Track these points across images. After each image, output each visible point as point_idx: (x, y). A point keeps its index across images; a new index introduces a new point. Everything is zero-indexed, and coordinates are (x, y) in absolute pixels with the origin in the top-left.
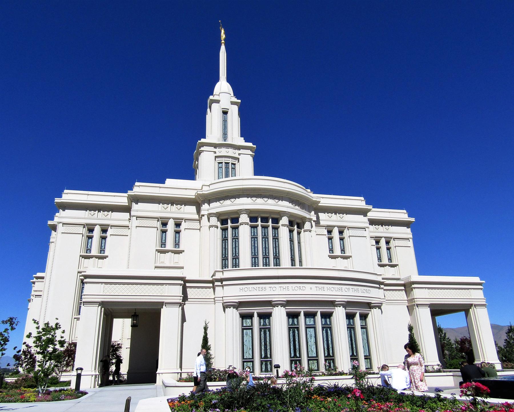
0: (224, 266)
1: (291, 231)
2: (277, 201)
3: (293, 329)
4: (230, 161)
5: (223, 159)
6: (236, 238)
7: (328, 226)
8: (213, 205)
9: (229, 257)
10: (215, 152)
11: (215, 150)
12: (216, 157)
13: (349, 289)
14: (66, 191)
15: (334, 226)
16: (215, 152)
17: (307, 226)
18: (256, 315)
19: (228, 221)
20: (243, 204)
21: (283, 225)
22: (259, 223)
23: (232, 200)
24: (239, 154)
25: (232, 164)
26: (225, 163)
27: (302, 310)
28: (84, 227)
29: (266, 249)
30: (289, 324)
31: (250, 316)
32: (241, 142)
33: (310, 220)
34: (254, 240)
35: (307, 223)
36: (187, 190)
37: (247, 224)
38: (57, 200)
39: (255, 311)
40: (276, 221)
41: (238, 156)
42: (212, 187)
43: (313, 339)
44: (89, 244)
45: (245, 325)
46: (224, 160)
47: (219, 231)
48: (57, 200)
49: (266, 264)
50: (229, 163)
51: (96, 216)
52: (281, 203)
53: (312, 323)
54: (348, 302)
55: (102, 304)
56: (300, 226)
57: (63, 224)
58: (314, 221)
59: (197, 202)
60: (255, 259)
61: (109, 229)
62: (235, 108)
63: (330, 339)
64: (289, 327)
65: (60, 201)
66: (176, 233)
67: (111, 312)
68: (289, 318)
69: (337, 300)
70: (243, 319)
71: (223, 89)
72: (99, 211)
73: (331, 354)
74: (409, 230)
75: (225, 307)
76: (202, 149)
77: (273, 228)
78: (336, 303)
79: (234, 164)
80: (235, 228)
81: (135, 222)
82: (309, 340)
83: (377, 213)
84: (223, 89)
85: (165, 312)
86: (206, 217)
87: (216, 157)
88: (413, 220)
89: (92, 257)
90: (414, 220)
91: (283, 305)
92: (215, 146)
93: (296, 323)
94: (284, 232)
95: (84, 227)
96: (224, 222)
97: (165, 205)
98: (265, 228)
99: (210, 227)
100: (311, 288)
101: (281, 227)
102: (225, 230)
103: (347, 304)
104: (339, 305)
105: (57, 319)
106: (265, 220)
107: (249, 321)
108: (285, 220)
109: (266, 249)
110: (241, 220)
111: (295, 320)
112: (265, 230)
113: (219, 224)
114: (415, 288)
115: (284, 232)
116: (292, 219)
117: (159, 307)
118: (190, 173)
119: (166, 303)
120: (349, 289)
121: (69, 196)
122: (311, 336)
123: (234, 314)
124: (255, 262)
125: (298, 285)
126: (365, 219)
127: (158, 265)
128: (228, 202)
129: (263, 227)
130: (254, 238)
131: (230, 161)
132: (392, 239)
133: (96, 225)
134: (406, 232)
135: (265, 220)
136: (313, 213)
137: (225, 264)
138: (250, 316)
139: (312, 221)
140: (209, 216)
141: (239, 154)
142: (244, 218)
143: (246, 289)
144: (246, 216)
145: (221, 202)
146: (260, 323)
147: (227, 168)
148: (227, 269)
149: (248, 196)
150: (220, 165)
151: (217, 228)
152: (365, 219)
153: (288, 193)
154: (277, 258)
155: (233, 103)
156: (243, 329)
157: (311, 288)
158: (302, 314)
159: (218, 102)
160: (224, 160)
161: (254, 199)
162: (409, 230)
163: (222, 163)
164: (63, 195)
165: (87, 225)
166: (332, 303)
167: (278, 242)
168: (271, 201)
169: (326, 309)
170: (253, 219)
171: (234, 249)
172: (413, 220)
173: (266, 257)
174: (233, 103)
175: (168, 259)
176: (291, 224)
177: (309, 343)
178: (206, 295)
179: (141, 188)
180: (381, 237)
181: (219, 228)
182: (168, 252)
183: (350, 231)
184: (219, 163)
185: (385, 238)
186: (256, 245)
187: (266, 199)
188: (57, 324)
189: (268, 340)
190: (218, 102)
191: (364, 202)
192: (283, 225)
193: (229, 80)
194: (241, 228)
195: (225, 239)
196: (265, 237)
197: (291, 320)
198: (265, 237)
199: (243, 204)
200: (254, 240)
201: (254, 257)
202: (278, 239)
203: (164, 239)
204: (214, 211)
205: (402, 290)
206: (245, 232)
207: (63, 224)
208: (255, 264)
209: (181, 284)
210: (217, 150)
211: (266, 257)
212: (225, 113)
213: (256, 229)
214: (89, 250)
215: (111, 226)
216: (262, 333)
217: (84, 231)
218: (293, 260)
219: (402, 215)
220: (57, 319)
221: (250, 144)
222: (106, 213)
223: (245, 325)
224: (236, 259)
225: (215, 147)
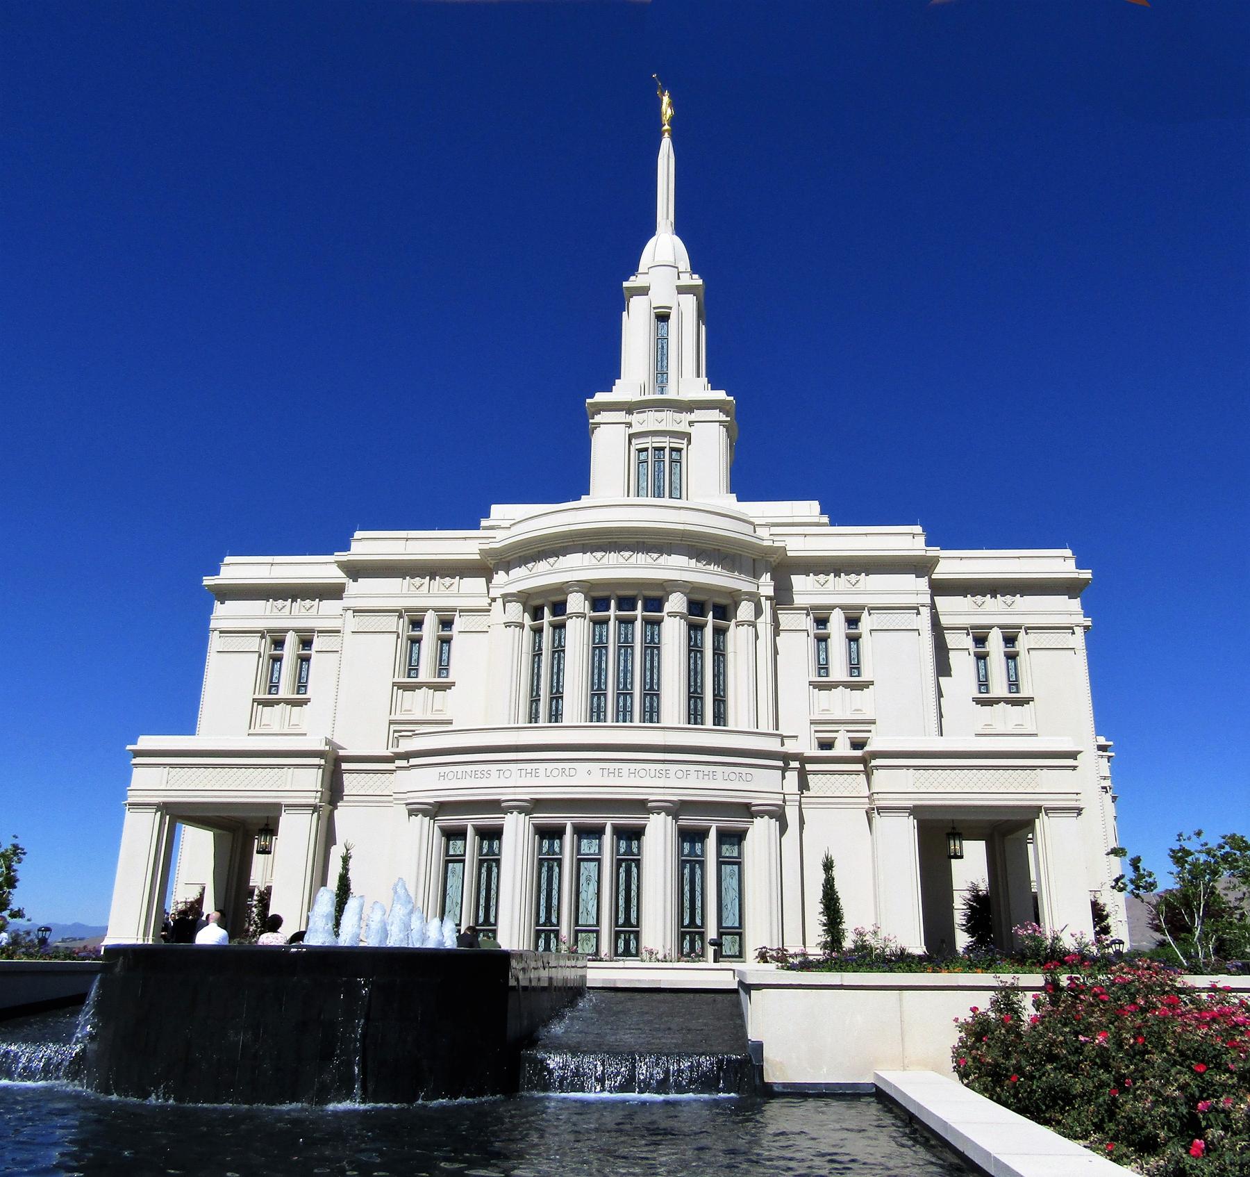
0: (533, 717)
1: (695, 629)
2: (656, 555)
3: (547, 865)
4: (665, 442)
5: (649, 439)
6: (559, 651)
7: (815, 608)
8: (516, 573)
9: (544, 700)
10: (629, 425)
11: (628, 419)
12: (631, 437)
13: (688, 773)
14: (358, 534)
15: (832, 608)
16: (629, 425)
17: (745, 611)
18: (608, 830)
19: (545, 607)
20: (572, 570)
21: (671, 614)
22: (612, 612)
23: (551, 560)
24: (691, 423)
25: (672, 449)
26: (656, 449)
27: (569, 821)
28: (400, 617)
29: (625, 674)
30: (480, 854)
31: (701, 835)
32: (699, 389)
33: (754, 598)
34: (600, 652)
35: (743, 603)
36: (468, 541)
37: (583, 616)
38: (208, 581)
39: (470, 822)
40: (655, 604)
41: (688, 429)
42: (515, 530)
43: (593, 887)
44: (276, 675)
45: (451, 852)
46: (648, 442)
47: (527, 634)
48: (208, 581)
49: (624, 713)
50: (663, 449)
51: (425, 589)
52: (666, 560)
53: (595, 849)
54: (683, 802)
55: (915, 811)
56: (724, 612)
57: (355, 611)
58: (768, 598)
59: (484, 568)
60: (599, 699)
61: (457, 619)
62: (689, 304)
63: (634, 887)
64: (618, 860)
65: (345, 559)
66: (303, 660)
67: (939, 833)
68: (542, 838)
69: (504, 798)
70: (448, 840)
71: (664, 259)
72: (432, 578)
73: (633, 921)
74: (1075, 604)
75: (412, 813)
76: (597, 419)
77: (647, 622)
78: (504, 804)
79: (679, 450)
80: (559, 627)
81: (351, 622)
82: (583, 888)
83: (957, 564)
84: (664, 259)
85: (287, 822)
86: (500, 601)
87: (631, 437)
88: (1087, 574)
89: (278, 702)
90: (1090, 576)
91: (521, 810)
92: (629, 408)
93: (557, 850)
94: (673, 633)
95: (400, 617)
96: (537, 614)
97: (418, 580)
98: (624, 622)
99: (508, 625)
100: (589, 772)
101: (666, 619)
102: (538, 631)
103: (677, 809)
104: (658, 810)
105: (15, 837)
106: (626, 603)
107: (460, 843)
108: (676, 602)
109: (625, 674)
110: (570, 609)
111: (635, 844)
112: (626, 628)
113: (527, 621)
114: (877, 767)
115: (673, 633)
116: (698, 597)
117: (1030, 817)
118: (570, 480)
119: (1047, 809)
120: (647, 772)
121: (238, 569)
122: (588, 880)
123: (423, 832)
124: (599, 705)
125: (633, 766)
126: (923, 583)
127: (398, 717)
128: (542, 566)
129: (621, 621)
130: (599, 648)
131: (665, 442)
132: (1023, 631)
133: (287, 631)
134: (1069, 609)
135: (626, 603)
136: (766, 578)
137: (599, 705)
138: (459, 834)
139: (763, 599)
140: (507, 598)
141: (691, 423)
142: (576, 602)
143: (642, 773)
144: (580, 596)
145: (530, 566)
146: (481, 848)
147: (660, 461)
148: (628, 724)
149: (584, 549)
150: (643, 456)
151: (522, 626)
152: (923, 583)
153: (684, 534)
154: (652, 694)
155: (682, 290)
156: (447, 862)
157: (589, 772)
158: (713, 834)
159: (644, 291)
160: (648, 442)
161: (599, 555)
162: (1075, 604)
163: (646, 450)
164: (353, 544)
165: (269, 631)
166: (641, 806)
167: (659, 655)
168: (641, 558)
169: (487, 820)
170: (599, 603)
171: (648, 673)
172: (1087, 574)
173: (624, 693)
174: (682, 290)
175: (417, 704)
176: (696, 607)
177: (583, 896)
178: (945, 784)
179: (369, 545)
180: (991, 627)
181: (527, 628)
182: (420, 688)
183: (874, 617)
184: (640, 451)
185: (1001, 627)
186: (604, 666)
187: (627, 554)
188: (16, 847)
189: (493, 886)
190: (644, 291)
191: (922, 539)
192: (671, 614)
193: (681, 229)
194: (570, 624)
195: (537, 654)
196: (625, 646)
197: (546, 843)
198: (625, 646)
199: (572, 570)
200: (600, 652)
201: (597, 692)
202: (658, 648)
203: (415, 656)
204: (513, 589)
205: (857, 772)
206: (577, 634)
207: (355, 611)
208: (596, 713)
209: (319, 766)
210: (635, 418)
211: (624, 693)
212: (663, 317)
213: (605, 626)
214: (273, 686)
215: (461, 611)
216: (484, 870)
217: (402, 625)
218: (694, 696)
219: (1058, 563)
220: (15, 837)
221: (721, 395)
222: (448, 580)
223: (451, 852)
224: (599, 696)
225: (630, 412)
